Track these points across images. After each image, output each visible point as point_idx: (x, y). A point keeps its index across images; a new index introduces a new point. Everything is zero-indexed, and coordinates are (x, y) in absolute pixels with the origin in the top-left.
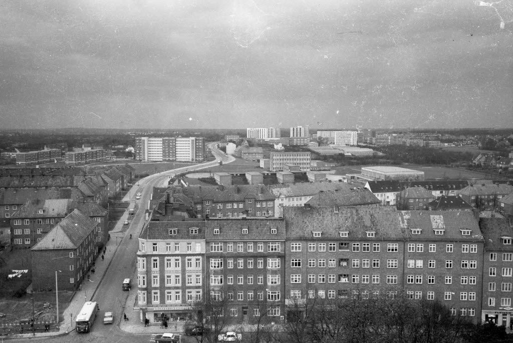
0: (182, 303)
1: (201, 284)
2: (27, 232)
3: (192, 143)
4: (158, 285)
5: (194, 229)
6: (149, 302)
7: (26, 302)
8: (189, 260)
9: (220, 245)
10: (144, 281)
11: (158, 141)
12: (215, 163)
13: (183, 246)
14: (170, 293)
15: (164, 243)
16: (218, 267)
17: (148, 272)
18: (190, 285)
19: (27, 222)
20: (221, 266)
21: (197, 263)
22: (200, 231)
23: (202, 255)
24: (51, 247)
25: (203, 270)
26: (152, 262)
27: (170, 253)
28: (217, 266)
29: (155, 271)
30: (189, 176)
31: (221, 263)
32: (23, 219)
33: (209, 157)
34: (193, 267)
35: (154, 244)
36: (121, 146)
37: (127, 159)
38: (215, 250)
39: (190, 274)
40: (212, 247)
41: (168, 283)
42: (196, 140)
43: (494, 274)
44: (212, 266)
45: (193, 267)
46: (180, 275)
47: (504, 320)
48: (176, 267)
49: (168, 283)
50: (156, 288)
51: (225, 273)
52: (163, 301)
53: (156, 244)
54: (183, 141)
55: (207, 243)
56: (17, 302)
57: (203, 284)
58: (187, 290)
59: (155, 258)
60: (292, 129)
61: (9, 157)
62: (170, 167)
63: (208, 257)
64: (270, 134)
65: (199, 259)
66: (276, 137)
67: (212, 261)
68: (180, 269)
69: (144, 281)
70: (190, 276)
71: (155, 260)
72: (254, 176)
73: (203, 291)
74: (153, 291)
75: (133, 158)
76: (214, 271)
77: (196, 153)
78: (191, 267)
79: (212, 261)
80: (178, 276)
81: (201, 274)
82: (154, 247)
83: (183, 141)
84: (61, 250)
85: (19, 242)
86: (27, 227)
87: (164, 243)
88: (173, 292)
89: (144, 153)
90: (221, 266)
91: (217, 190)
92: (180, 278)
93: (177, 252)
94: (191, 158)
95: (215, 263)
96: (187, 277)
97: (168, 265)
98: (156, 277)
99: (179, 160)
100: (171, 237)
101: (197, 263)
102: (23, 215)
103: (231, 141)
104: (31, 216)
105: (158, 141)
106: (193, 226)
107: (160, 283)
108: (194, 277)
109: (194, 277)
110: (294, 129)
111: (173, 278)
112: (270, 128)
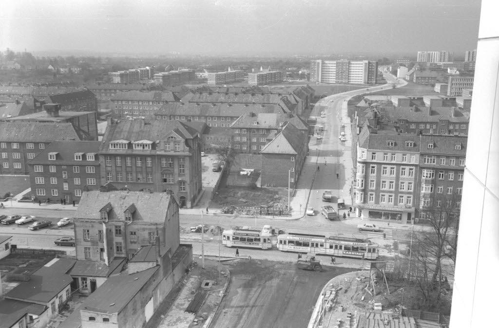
0: (394, 205)
1: (412, 191)
2: (245, 139)
3: (366, 66)
4: (374, 188)
5: (410, 142)
6: (365, 201)
7: (259, 193)
8: (403, 169)
9: (433, 158)
10: (362, 183)
11: (356, 64)
12: (387, 87)
13: (398, 158)
14: (384, 195)
15: (383, 153)
16: (430, 177)
17: (366, 177)
18: (384, 189)
19: (244, 132)
20: (433, 177)
21: (410, 172)
22: (415, 145)
23: (416, 166)
24: (277, 151)
25: (415, 179)
26: (371, 168)
27: (387, 162)
28: (429, 176)
29: (373, 176)
30: (366, 97)
31: (433, 174)
32: (241, 129)
33: (380, 80)
34: (406, 176)
35: (373, 153)
36: (295, 69)
37: (301, 81)
38: (428, 162)
39: (403, 181)
40: (425, 159)
41: (383, 187)
42: (369, 63)
43: (403, 189)
44: (424, 176)
45: (406, 176)
46: (394, 181)
47: (287, 243)
48: (391, 174)
49: (383, 187)
50: (372, 191)
51: (434, 183)
52: (377, 202)
53: (374, 154)
54: (359, 64)
55: (422, 155)
56: (253, 193)
57: (414, 191)
58: (399, 195)
59: (373, 165)
60: (467, 52)
61: (201, 76)
62: (345, 90)
63: (420, 168)
64: (443, 57)
65: (393, 168)
66: (449, 61)
67: (425, 172)
68: (394, 175)
69: (362, 183)
70: (385, 182)
71: (373, 167)
72: (433, 100)
73: (414, 196)
74: (370, 193)
75: (306, 79)
76: (426, 180)
77: (368, 76)
78: (404, 175)
79: (425, 172)
80: (392, 182)
81: (413, 182)
82: (373, 156)
83: (359, 64)
84: (285, 154)
85: (237, 147)
86: (244, 135)
87: (383, 153)
88: (387, 195)
89: (318, 75)
90: (433, 177)
91: (411, 111)
92: (394, 184)
93: (393, 162)
94: (363, 81)
95: (427, 174)
96: (400, 183)
97: (372, 171)
98: (373, 181)
99: (351, 83)
100: (389, 148)
101: (410, 172)
102: (241, 126)
103: (401, 65)
104: (248, 127)
105: (356, 64)
106: (409, 140)
107: (395, 188)
108: (406, 185)
109: (406, 185)
110: (469, 53)
111: (387, 184)
112: (443, 51)
